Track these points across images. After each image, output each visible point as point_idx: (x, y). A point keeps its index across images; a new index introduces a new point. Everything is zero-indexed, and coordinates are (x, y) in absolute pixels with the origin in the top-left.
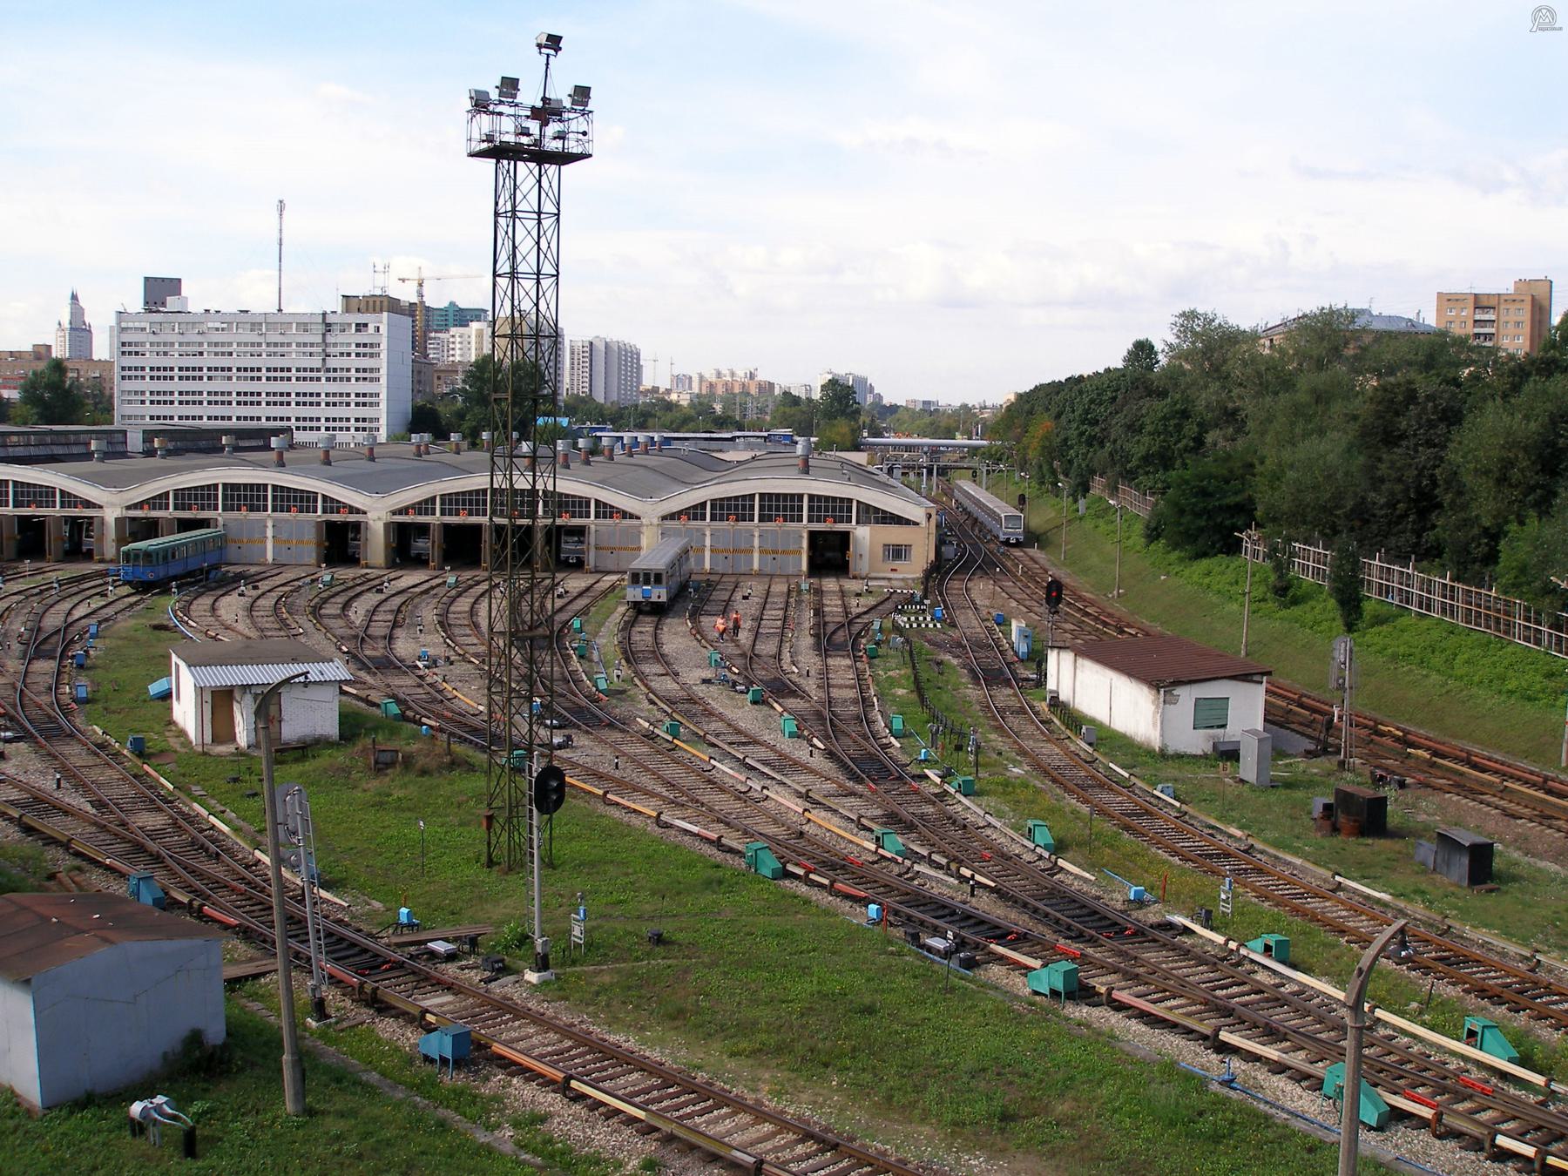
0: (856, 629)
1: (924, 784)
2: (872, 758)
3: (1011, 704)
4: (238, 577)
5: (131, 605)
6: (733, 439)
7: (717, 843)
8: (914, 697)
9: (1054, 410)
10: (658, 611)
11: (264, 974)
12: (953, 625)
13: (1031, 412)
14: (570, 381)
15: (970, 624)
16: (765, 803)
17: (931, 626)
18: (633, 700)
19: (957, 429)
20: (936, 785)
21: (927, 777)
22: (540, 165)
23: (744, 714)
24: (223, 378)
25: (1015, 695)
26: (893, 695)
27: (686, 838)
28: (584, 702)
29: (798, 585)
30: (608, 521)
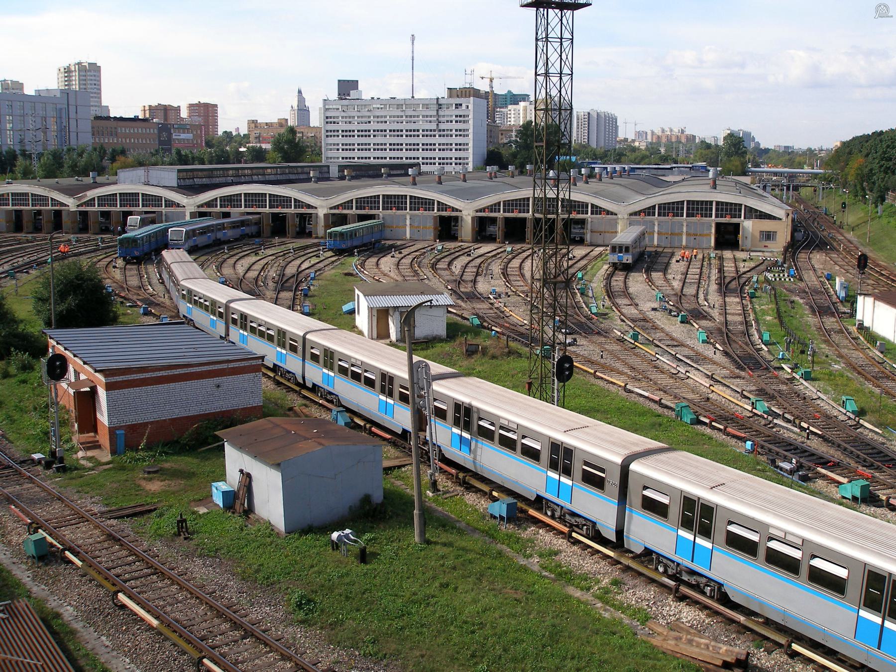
0: (742, 281)
1: (781, 373)
2: (751, 357)
3: (834, 327)
4: (391, 247)
5: (333, 262)
6: (671, 168)
7: (659, 403)
8: (776, 321)
9: (865, 152)
10: (627, 268)
11: (404, 466)
12: (801, 280)
13: (850, 153)
14: (577, 135)
15: (810, 279)
16: (687, 380)
17: (787, 280)
18: (612, 319)
19: (805, 163)
20: (789, 373)
21: (783, 368)
22: (561, 10)
23: (674, 328)
24: (382, 136)
25: (837, 322)
26: (764, 320)
27: (641, 399)
28: (583, 320)
29: (709, 254)
30: (598, 216)
